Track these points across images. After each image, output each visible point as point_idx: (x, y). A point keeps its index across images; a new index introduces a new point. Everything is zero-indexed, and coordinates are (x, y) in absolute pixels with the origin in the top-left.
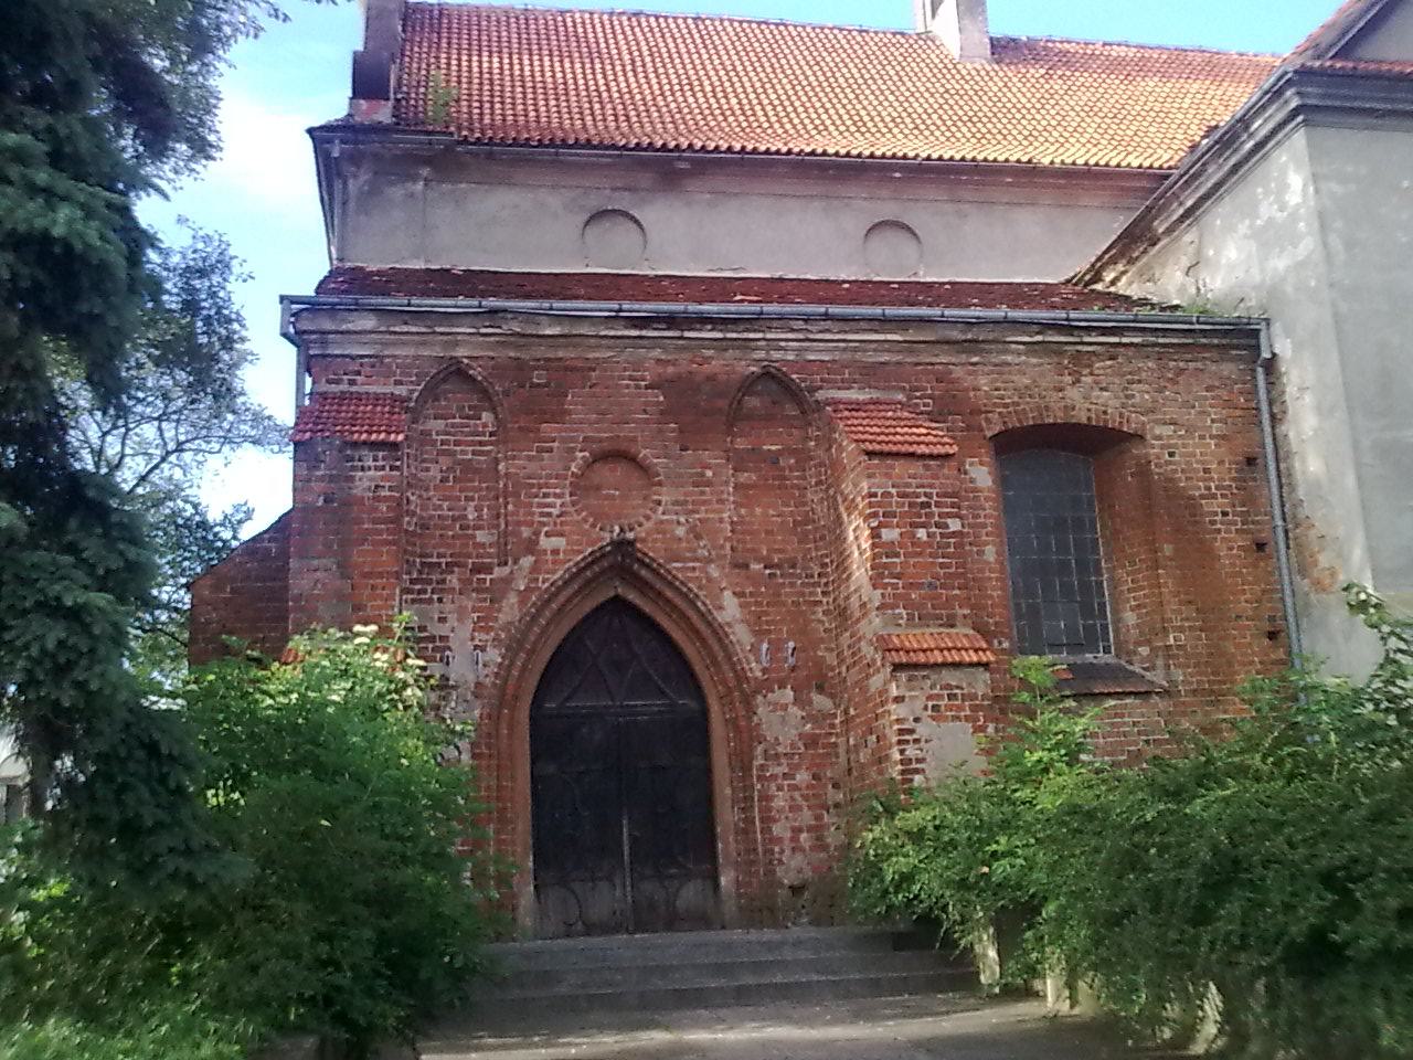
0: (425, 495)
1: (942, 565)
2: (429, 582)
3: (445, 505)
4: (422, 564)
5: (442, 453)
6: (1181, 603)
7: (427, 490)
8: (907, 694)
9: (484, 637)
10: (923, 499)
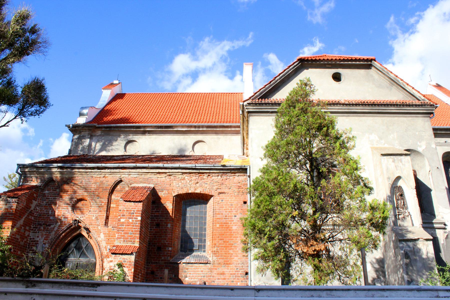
0: (42, 208)
1: (134, 229)
2: (37, 228)
3: (45, 210)
4: (38, 224)
5: (47, 198)
6: (219, 240)
7: (42, 207)
8: (113, 260)
9: (46, 241)
10: (132, 212)
